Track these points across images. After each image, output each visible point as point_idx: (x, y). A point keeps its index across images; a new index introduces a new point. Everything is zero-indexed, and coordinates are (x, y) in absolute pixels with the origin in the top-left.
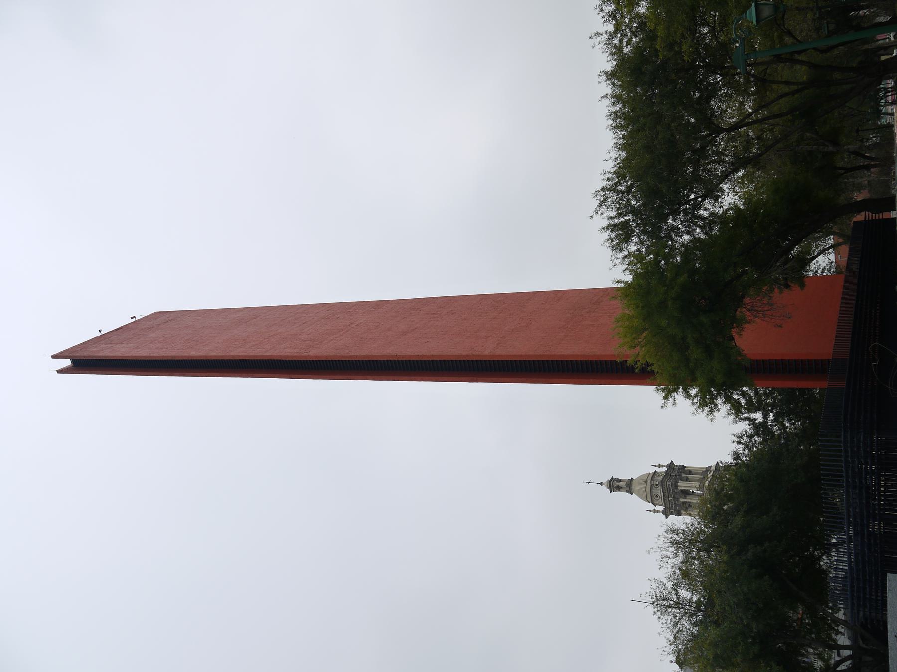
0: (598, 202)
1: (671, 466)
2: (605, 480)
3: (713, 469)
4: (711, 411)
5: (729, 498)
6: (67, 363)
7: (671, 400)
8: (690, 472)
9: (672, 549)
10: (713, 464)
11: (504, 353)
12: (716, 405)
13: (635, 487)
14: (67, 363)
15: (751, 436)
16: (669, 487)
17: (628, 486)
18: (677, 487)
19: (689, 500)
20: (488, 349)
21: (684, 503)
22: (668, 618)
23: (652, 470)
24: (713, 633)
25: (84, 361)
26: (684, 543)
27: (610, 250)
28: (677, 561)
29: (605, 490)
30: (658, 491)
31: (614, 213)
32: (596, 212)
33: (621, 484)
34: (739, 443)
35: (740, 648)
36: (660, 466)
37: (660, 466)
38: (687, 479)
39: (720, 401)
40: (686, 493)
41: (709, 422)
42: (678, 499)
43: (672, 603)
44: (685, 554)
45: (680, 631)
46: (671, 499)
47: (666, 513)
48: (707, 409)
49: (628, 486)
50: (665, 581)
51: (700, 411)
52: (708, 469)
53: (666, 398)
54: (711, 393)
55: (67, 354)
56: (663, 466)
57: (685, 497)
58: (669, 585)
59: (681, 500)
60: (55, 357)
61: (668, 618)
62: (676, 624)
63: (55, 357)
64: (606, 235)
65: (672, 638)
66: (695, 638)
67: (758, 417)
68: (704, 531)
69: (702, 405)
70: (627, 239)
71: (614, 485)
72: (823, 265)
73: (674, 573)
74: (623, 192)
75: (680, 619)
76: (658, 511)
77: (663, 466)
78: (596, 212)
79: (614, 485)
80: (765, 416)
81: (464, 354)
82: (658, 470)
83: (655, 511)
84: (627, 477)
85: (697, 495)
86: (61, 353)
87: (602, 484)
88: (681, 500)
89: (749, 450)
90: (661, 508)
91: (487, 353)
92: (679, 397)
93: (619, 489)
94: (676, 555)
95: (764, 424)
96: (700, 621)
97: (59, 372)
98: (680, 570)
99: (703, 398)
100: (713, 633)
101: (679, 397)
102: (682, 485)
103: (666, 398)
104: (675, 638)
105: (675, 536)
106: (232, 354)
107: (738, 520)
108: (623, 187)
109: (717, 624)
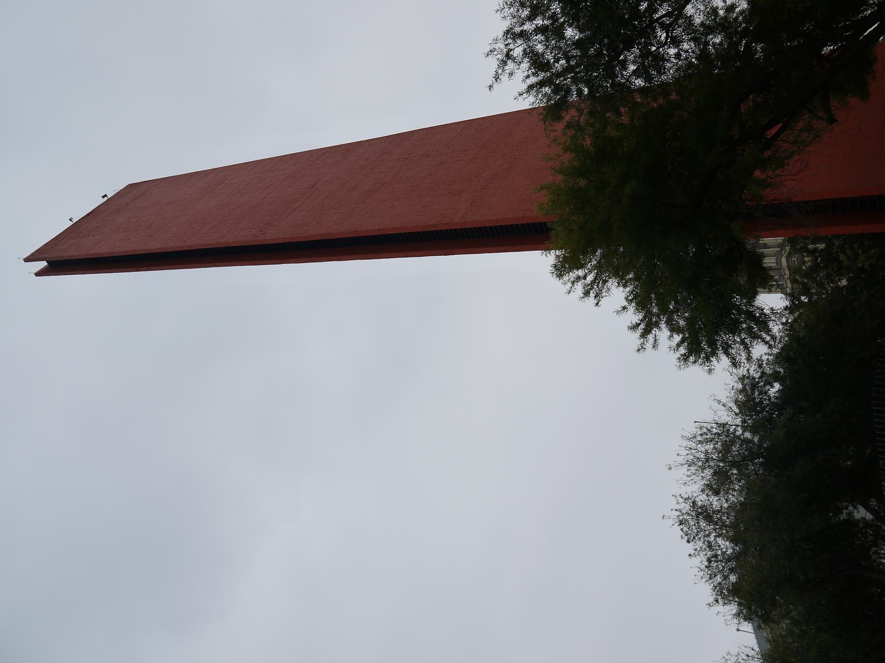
6: (43, 264)
7: (651, 337)
14: (43, 264)
25: (63, 258)
26: (726, 460)
32: (497, 78)
60: (27, 260)
63: (27, 260)
86: (32, 255)
92: (663, 333)
97: (38, 274)
101: (663, 333)
105: (747, 341)
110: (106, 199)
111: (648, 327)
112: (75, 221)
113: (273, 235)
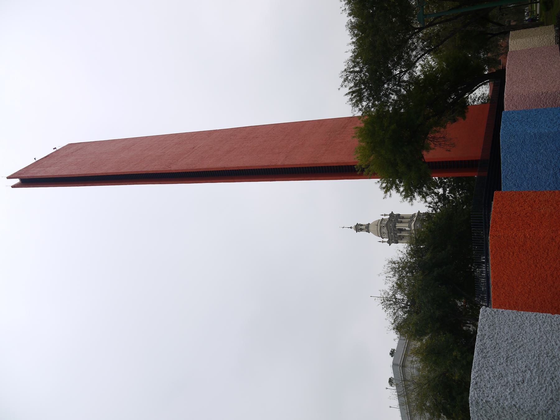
0: (343, 80)
1: (392, 215)
2: (353, 226)
3: (416, 215)
4: (411, 200)
5: (423, 242)
6: (17, 181)
7: (388, 193)
8: (403, 218)
9: (393, 273)
10: (417, 212)
11: (290, 163)
12: (414, 197)
13: (370, 228)
14: (17, 181)
15: (436, 203)
16: (391, 228)
17: (367, 228)
18: (395, 227)
19: (403, 234)
20: (280, 161)
21: (399, 236)
22: (390, 311)
23: (380, 218)
24: (415, 318)
25: (28, 179)
26: (401, 269)
27: (350, 106)
28: (395, 279)
29: (353, 231)
30: (385, 230)
31: (352, 85)
32: (342, 86)
33: (362, 227)
34: (429, 207)
35: (429, 325)
36: (385, 215)
37: (385, 215)
38: (401, 222)
39: (416, 194)
40: (401, 230)
41: (410, 206)
42: (396, 234)
43: (392, 302)
44: (400, 276)
45: (397, 317)
46: (392, 234)
47: (390, 243)
48: (409, 199)
49: (367, 228)
50: (389, 291)
51: (405, 200)
52: (414, 215)
53: (386, 192)
54: (411, 190)
55: (16, 176)
56: (387, 215)
57: (401, 233)
58: (391, 293)
59: (398, 234)
60: (9, 178)
61: (390, 311)
62: (395, 314)
63: (9, 178)
64: (349, 96)
65: (393, 321)
66: (405, 320)
67: (441, 191)
68: (410, 262)
69: (406, 197)
70: (361, 100)
71: (359, 228)
72: (479, 95)
73: (393, 286)
74: (357, 72)
75: (397, 310)
76: (385, 242)
77: (387, 215)
78: (342, 86)
79: (359, 228)
80: (445, 191)
81: (266, 164)
82: (384, 217)
83: (383, 242)
84: (365, 223)
85: (408, 231)
86: (12, 175)
87: (351, 228)
88: (398, 234)
89: (436, 211)
90: (387, 240)
91: (279, 163)
92: (393, 192)
93: (361, 230)
94: (394, 275)
95: (444, 194)
96: (408, 311)
97: (13, 187)
98: (397, 283)
99: (407, 193)
100: (415, 318)
101: (393, 192)
102: (399, 226)
103: (386, 192)
104: (395, 321)
105: (393, 265)
106: (122, 171)
107: (428, 256)
108: (357, 69)
109: (417, 313)
110: (55, 150)
111: (387, 189)
112: (37, 160)
113: (176, 167)
